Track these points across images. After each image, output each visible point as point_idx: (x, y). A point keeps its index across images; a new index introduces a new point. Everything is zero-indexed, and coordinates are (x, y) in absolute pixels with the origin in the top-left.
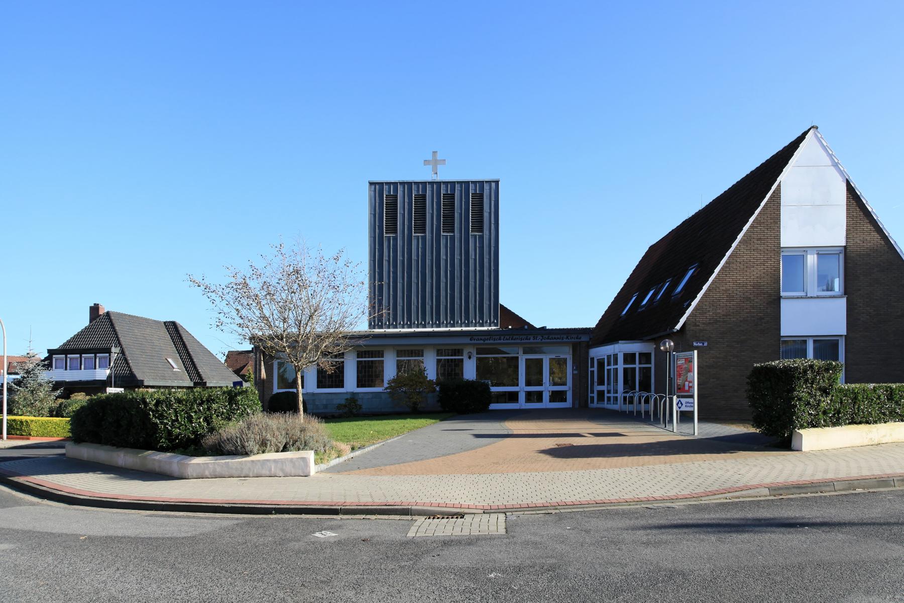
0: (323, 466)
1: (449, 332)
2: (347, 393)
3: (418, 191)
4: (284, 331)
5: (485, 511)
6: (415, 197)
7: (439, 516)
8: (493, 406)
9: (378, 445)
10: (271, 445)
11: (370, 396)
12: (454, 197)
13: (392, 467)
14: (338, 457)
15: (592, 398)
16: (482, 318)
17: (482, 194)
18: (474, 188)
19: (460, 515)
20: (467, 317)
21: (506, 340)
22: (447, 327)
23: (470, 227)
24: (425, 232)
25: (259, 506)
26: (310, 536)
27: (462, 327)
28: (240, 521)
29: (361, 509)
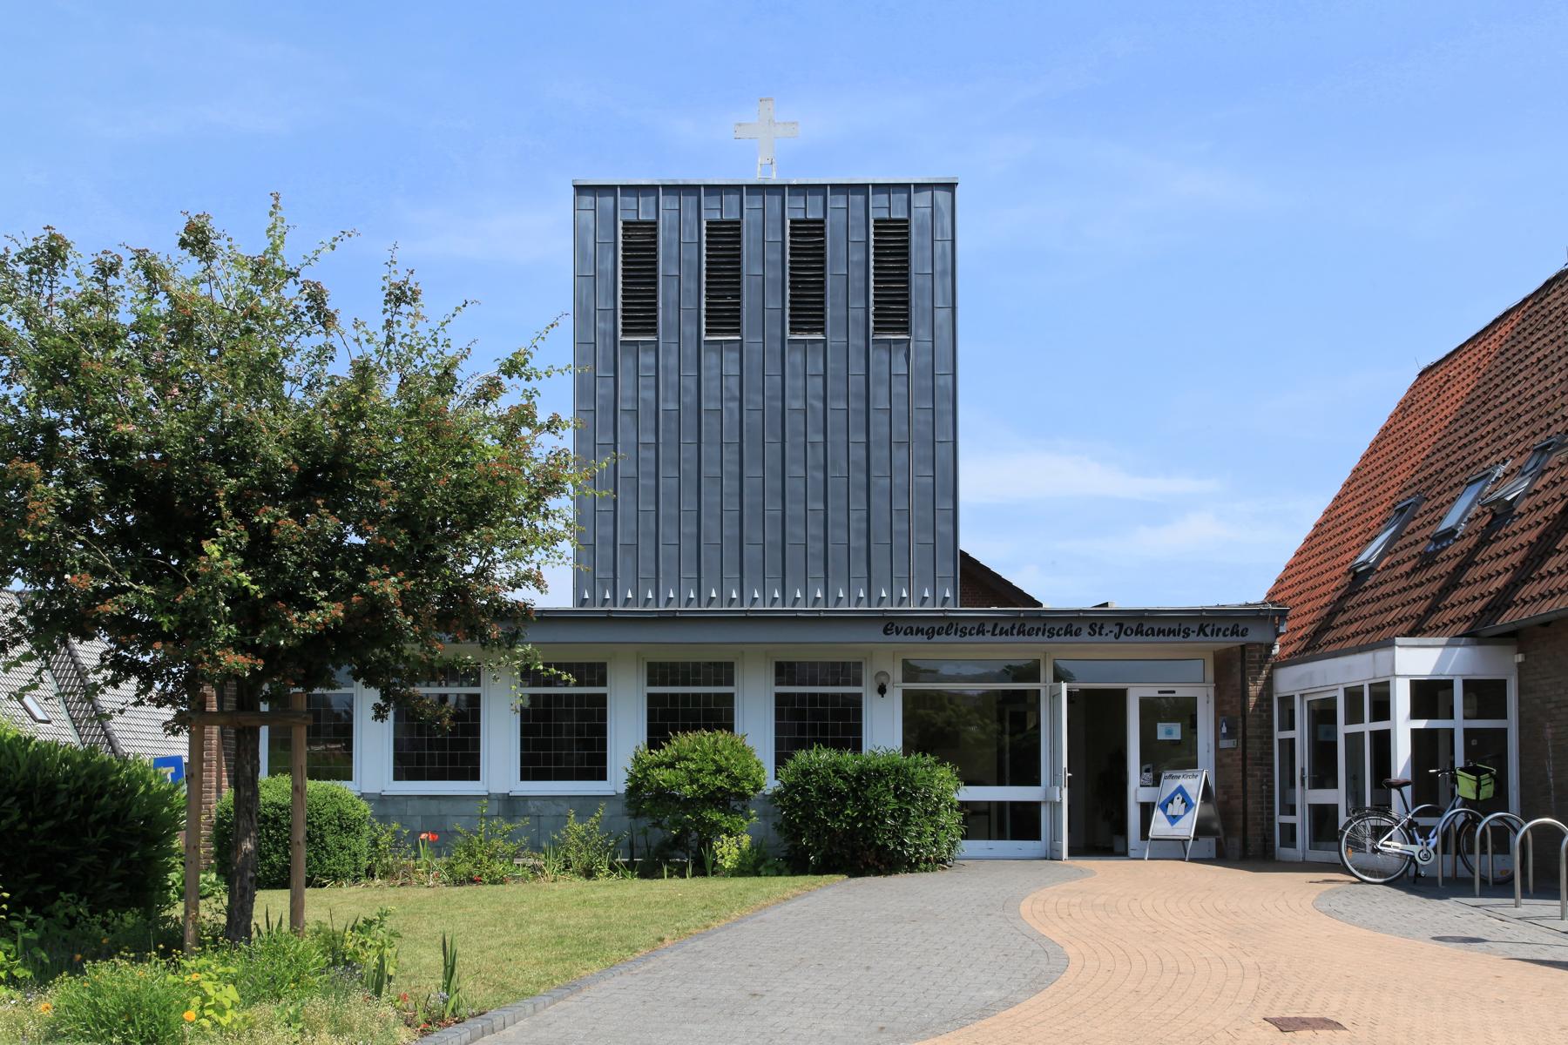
15: (1290, 833)
21: (1001, 634)
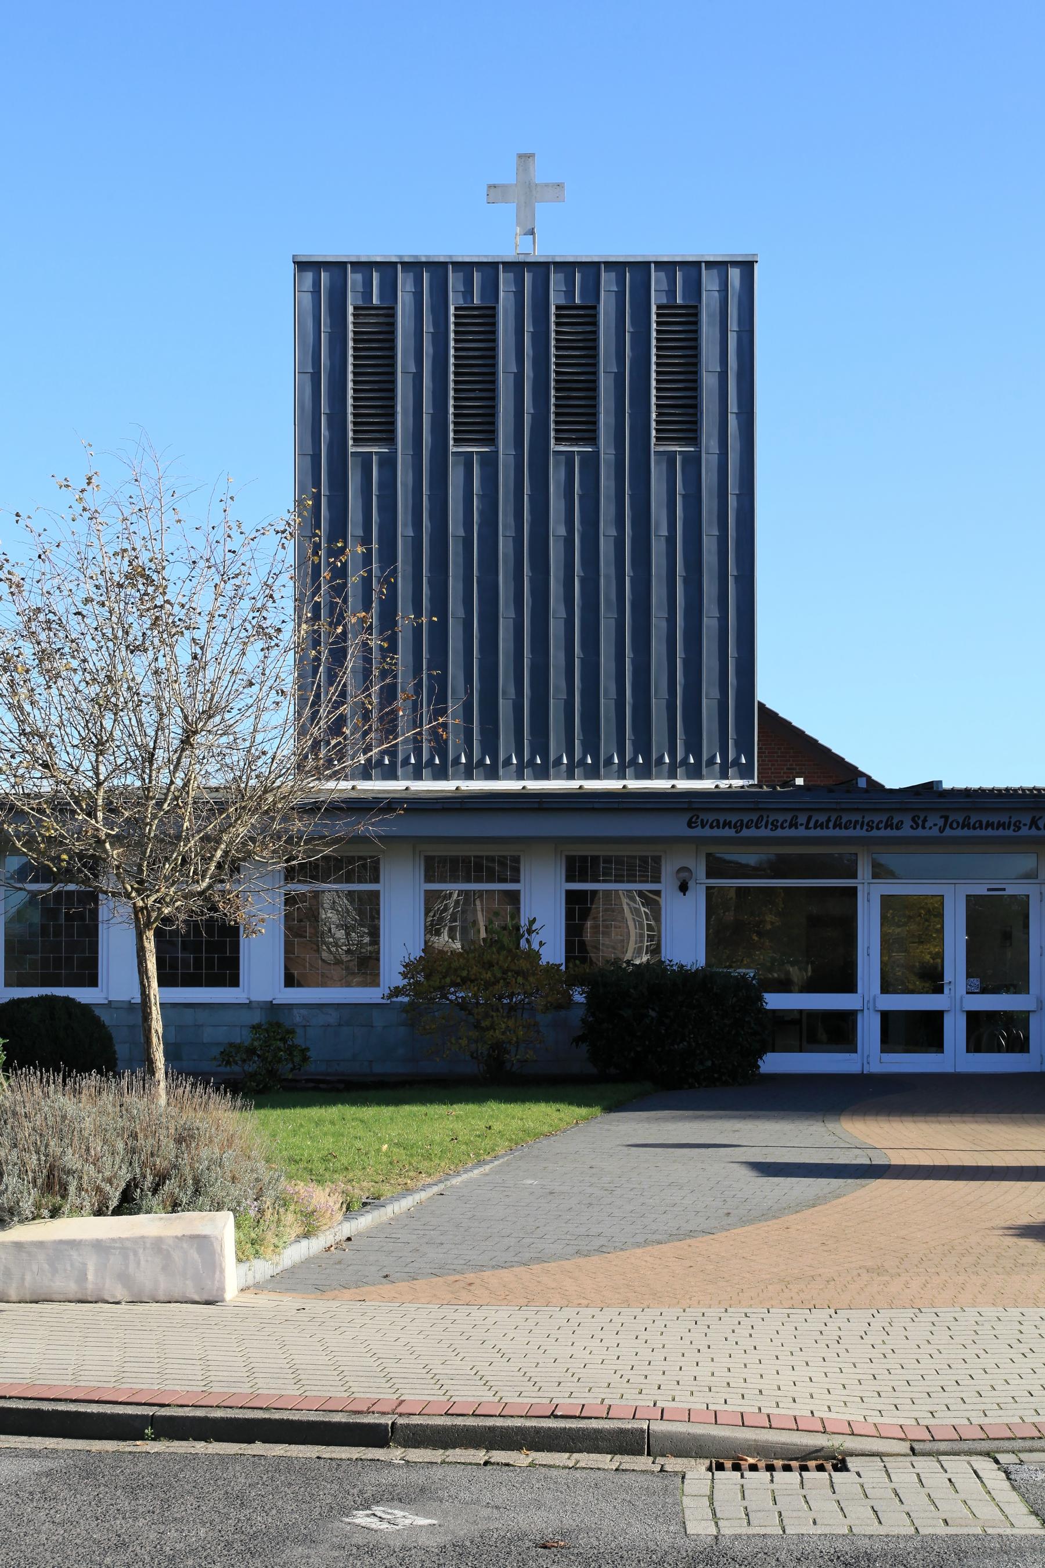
0: (262, 1268)
1: (582, 795)
2: (249, 1006)
3: (468, 292)
4: (99, 784)
5: (917, 1446)
6: (456, 316)
7: (751, 1461)
8: (773, 1063)
9: (423, 1196)
10: (80, 1188)
11: (332, 1018)
12: (595, 316)
13: (505, 1274)
14: (307, 1235)
16: (694, 745)
17: (696, 307)
18: (665, 287)
19: (827, 1459)
20: (643, 745)
21: (815, 827)
22: (571, 776)
23: (653, 425)
24: (492, 441)
25: (94, 1409)
26: (337, 1524)
27: (625, 778)
28: (49, 1464)
29: (467, 1429)
